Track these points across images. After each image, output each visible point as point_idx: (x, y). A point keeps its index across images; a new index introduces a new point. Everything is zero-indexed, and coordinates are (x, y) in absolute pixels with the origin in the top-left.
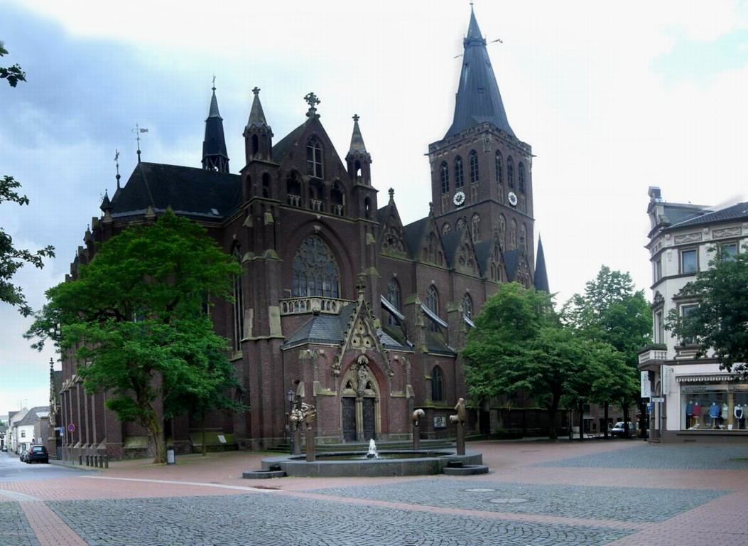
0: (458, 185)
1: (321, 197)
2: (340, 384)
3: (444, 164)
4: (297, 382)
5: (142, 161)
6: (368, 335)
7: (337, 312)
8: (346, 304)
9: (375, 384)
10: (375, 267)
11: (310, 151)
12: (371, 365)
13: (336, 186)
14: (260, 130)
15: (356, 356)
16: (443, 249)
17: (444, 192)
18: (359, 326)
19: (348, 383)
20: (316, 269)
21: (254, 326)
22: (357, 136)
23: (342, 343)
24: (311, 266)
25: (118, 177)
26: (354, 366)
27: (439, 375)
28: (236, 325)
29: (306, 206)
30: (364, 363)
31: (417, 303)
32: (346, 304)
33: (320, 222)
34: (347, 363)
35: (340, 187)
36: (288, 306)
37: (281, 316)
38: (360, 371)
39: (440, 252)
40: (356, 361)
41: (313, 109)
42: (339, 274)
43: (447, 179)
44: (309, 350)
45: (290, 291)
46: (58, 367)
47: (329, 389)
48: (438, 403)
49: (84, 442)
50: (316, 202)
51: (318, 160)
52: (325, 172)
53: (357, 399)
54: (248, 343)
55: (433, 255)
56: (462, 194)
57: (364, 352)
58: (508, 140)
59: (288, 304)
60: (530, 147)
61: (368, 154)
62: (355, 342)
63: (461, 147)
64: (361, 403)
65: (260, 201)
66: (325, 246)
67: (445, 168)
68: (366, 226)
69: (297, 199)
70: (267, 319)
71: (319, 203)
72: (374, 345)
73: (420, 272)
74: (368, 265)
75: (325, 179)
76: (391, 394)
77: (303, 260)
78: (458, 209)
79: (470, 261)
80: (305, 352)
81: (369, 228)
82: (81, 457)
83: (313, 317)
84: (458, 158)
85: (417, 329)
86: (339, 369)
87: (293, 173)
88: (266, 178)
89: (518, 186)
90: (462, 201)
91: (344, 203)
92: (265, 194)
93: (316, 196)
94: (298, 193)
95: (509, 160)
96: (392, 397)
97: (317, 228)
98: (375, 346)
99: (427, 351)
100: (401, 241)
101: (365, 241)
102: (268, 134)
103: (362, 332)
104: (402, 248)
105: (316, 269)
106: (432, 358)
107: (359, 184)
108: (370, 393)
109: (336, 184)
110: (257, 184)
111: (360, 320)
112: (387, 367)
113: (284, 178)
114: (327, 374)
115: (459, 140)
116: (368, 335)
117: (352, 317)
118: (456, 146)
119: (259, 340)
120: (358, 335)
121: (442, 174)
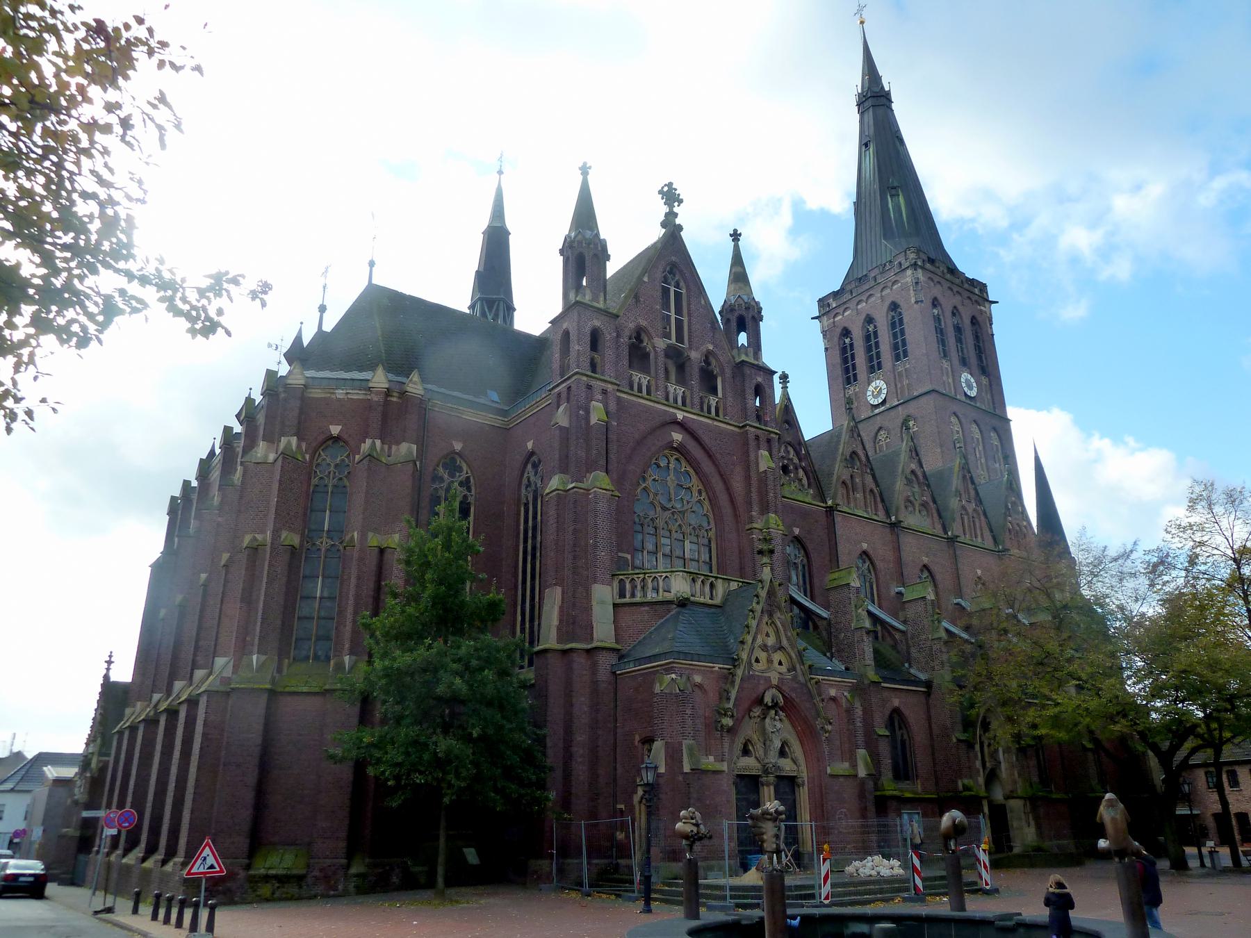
0: (872, 370)
1: (682, 381)
2: (731, 750)
3: (846, 332)
4: (648, 741)
5: (374, 282)
6: (781, 648)
7: (718, 600)
8: (734, 586)
9: (796, 748)
10: (776, 512)
11: (666, 292)
12: (788, 707)
13: (707, 362)
14: (589, 244)
15: (761, 688)
16: (877, 485)
17: (849, 383)
18: (765, 628)
19: (745, 745)
20: (673, 513)
21: (561, 621)
22: (739, 269)
23: (735, 662)
24: (664, 509)
25: (322, 309)
26: (757, 711)
27: (900, 728)
28: (519, 618)
29: (660, 395)
30: (775, 705)
31: (852, 584)
32: (734, 586)
33: (682, 426)
34: (746, 705)
35: (713, 362)
36: (628, 586)
37: (615, 606)
38: (767, 720)
39: (871, 491)
40: (760, 701)
41: (671, 215)
42: (713, 525)
43: (853, 359)
44: (673, 676)
45: (629, 557)
46: (124, 673)
47: (711, 758)
48: (904, 785)
49: (151, 850)
50: (676, 390)
51: (679, 311)
52: (690, 336)
53: (764, 779)
54: (549, 655)
55: (859, 495)
56: (881, 384)
57: (775, 682)
58: (948, 276)
59: (627, 582)
60: (985, 286)
61: (757, 303)
62: (757, 661)
63: (872, 299)
64: (772, 788)
65: (585, 378)
66: (687, 472)
67: (847, 341)
68: (757, 438)
69: (645, 383)
70: (588, 609)
71: (680, 391)
72: (792, 669)
73: (843, 528)
74: (765, 510)
75: (690, 348)
76: (829, 771)
77: (651, 495)
78: (877, 411)
79: (924, 505)
80: (668, 678)
81: (763, 443)
82: (138, 894)
83: (675, 610)
84: (869, 320)
85: (858, 634)
86: (732, 716)
87: (639, 334)
88: (595, 340)
89: (973, 360)
90: (883, 396)
91: (720, 395)
92: (593, 367)
93: (673, 377)
94: (645, 370)
95: (954, 314)
96: (832, 776)
97: (677, 437)
98: (794, 669)
99: (876, 678)
100: (803, 469)
101: (757, 464)
102: (601, 253)
103: (771, 641)
104: (805, 481)
105: (673, 513)
106: (886, 694)
107: (743, 358)
108: (787, 766)
109: (706, 356)
110: (579, 347)
111: (766, 619)
112: (818, 715)
113: (624, 340)
114: (707, 726)
115: (866, 287)
116: (781, 648)
117: (752, 611)
118: (864, 298)
119: (571, 650)
120: (764, 648)
121: (844, 350)
